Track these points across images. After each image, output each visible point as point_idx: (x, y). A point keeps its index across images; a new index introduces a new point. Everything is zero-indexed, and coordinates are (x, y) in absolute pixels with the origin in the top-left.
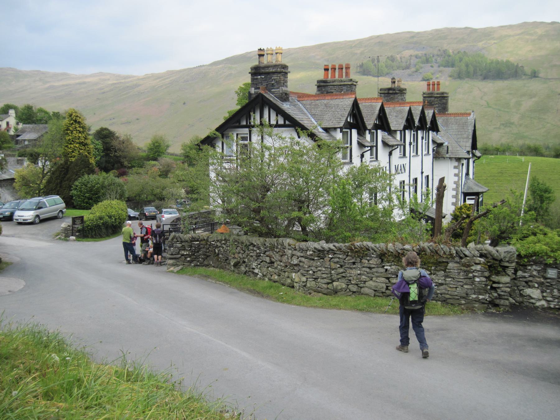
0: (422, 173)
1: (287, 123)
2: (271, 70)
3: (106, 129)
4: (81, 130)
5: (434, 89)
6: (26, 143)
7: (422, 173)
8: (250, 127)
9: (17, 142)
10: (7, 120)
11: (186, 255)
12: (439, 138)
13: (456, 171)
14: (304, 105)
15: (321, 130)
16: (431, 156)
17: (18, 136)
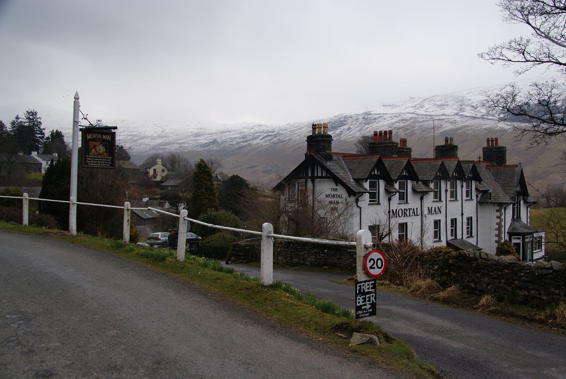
0: (462, 214)
1: (328, 175)
3: (237, 176)
5: (492, 144)
6: (169, 188)
7: (462, 214)
8: (306, 178)
9: (162, 188)
10: (155, 167)
13: (498, 214)
14: (346, 163)
16: (474, 202)
17: (163, 182)
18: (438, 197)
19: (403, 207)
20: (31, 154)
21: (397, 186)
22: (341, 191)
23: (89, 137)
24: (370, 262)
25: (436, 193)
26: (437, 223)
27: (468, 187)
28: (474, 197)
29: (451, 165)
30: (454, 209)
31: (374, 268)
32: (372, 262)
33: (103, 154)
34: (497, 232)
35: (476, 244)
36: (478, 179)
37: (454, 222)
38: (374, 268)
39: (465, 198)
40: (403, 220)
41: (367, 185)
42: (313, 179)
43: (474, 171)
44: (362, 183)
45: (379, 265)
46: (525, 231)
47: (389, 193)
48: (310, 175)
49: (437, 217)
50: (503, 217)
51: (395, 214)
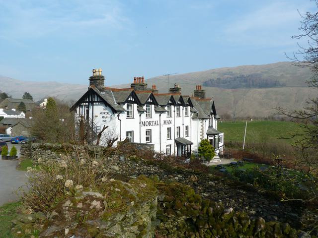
2: (97, 78)
12: (195, 109)
13: (202, 124)
15: (116, 103)
19: (149, 120)
21: (145, 108)
26: (169, 129)
28: (189, 115)
29: (177, 98)
30: (178, 122)
34: (201, 134)
36: (191, 105)
39: (184, 115)
40: (149, 128)
41: (125, 107)
43: (189, 101)
46: (215, 133)
47: (141, 112)
50: (204, 126)
51: (144, 124)
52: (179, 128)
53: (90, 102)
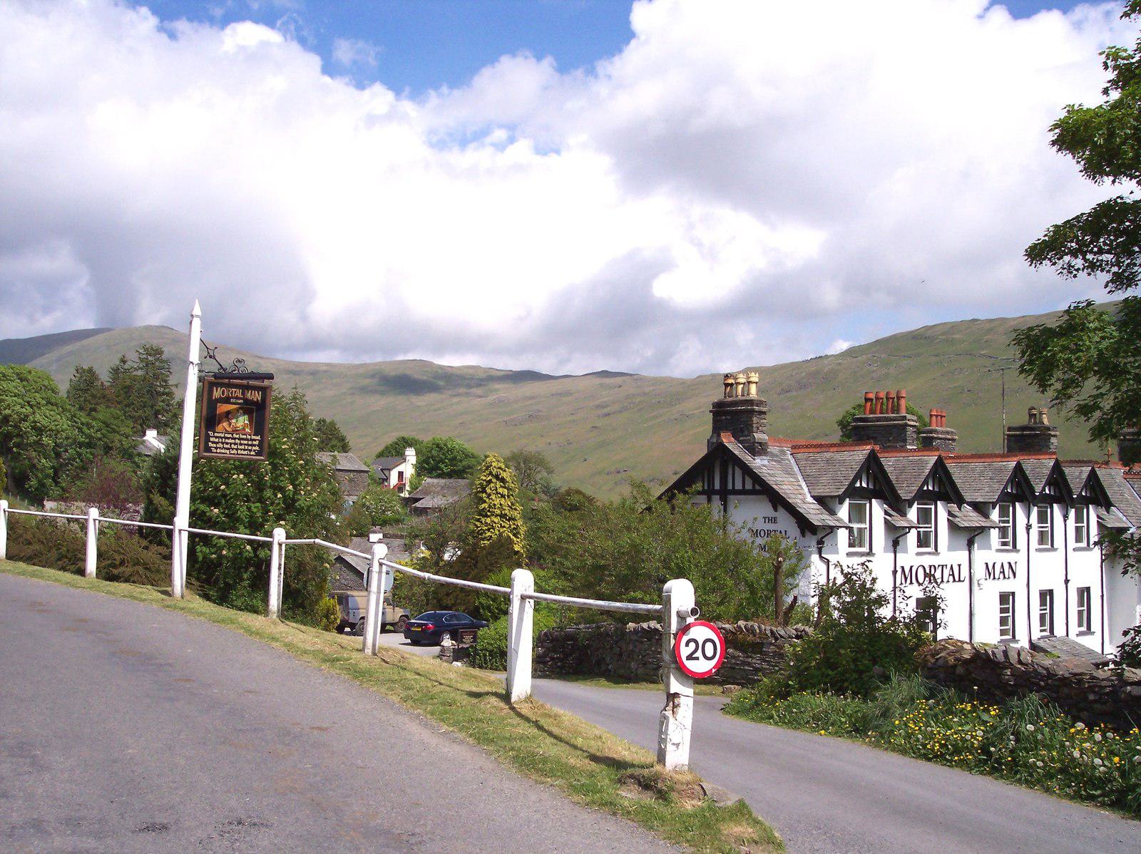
0: (1067, 581)
1: (757, 487)
4: (506, 492)
7: (1067, 581)
10: (401, 468)
11: (557, 658)
12: (1116, 519)
15: (810, 499)
17: (417, 500)
18: (1009, 543)
19: (928, 561)
20: (144, 434)
21: (912, 514)
22: (785, 523)
23: (217, 393)
24: (687, 645)
25: (1003, 532)
26: (1006, 599)
27: (1079, 519)
30: (1046, 570)
31: (697, 659)
32: (692, 645)
33: (244, 429)
35: (1100, 652)
37: (1047, 596)
38: (697, 659)
41: (843, 512)
42: (724, 494)
44: (831, 506)
45: (709, 652)
48: (717, 486)
49: (1006, 586)
52: (1047, 596)
53: (716, 492)
